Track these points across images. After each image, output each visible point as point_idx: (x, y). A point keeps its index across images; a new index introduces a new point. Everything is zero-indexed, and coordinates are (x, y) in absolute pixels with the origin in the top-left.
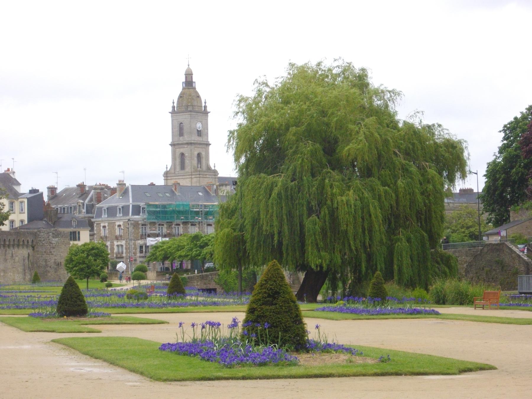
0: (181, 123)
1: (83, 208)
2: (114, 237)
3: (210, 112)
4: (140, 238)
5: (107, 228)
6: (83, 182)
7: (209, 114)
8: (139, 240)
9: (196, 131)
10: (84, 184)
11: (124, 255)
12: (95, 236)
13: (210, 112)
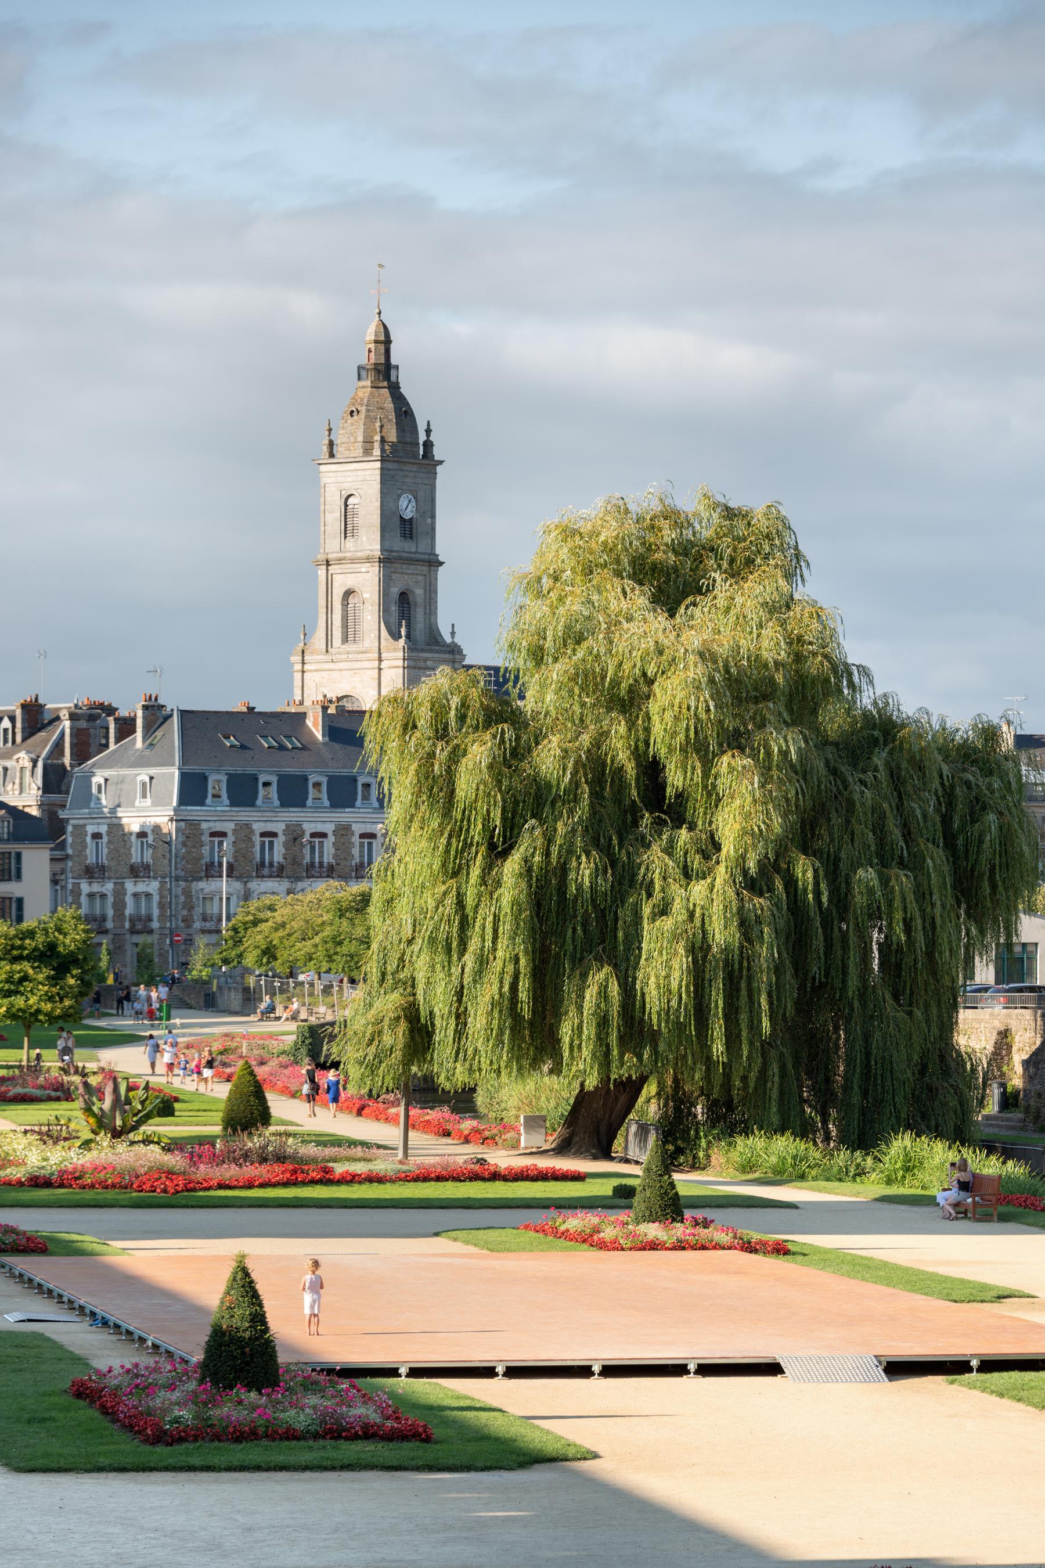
3: (441, 462)
7: (439, 468)
8: (200, 879)
9: (398, 521)
13: (441, 462)
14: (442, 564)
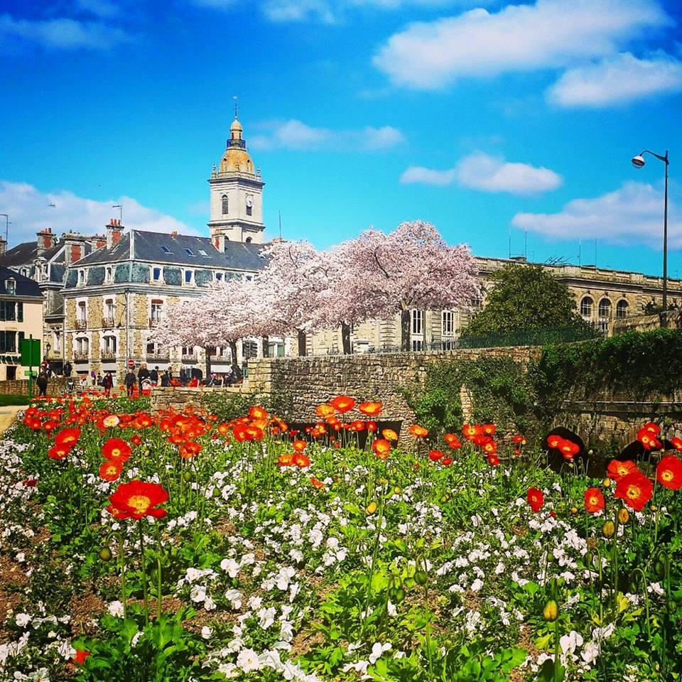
0: (225, 196)
1: (47, 272)
2: (100, 325)
4: (148, 325)
5: (87, 305)
6: (50, 229)
10: (53, 233)
11: (117, 355)
12: (66, 321)
14: (264, 228)
